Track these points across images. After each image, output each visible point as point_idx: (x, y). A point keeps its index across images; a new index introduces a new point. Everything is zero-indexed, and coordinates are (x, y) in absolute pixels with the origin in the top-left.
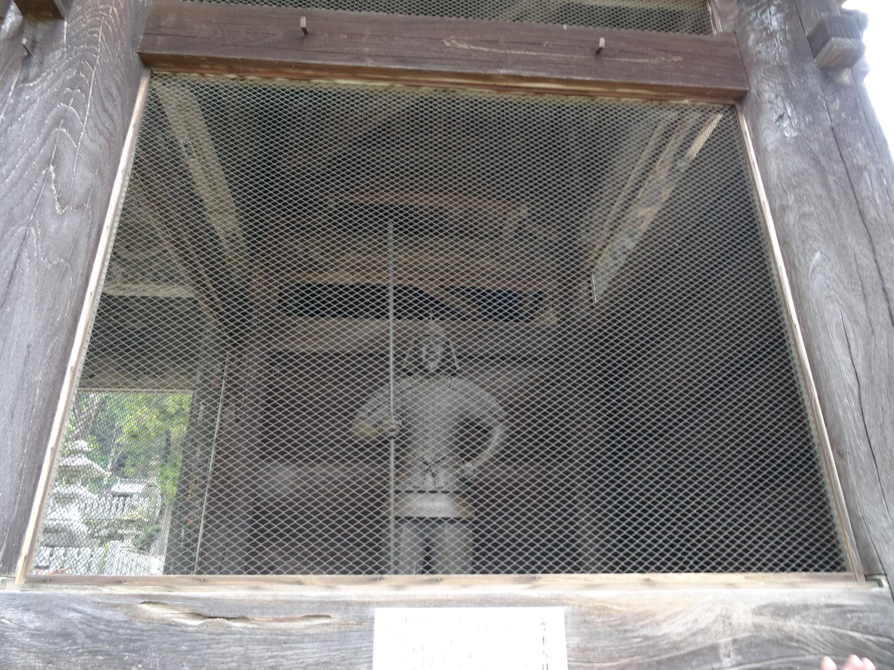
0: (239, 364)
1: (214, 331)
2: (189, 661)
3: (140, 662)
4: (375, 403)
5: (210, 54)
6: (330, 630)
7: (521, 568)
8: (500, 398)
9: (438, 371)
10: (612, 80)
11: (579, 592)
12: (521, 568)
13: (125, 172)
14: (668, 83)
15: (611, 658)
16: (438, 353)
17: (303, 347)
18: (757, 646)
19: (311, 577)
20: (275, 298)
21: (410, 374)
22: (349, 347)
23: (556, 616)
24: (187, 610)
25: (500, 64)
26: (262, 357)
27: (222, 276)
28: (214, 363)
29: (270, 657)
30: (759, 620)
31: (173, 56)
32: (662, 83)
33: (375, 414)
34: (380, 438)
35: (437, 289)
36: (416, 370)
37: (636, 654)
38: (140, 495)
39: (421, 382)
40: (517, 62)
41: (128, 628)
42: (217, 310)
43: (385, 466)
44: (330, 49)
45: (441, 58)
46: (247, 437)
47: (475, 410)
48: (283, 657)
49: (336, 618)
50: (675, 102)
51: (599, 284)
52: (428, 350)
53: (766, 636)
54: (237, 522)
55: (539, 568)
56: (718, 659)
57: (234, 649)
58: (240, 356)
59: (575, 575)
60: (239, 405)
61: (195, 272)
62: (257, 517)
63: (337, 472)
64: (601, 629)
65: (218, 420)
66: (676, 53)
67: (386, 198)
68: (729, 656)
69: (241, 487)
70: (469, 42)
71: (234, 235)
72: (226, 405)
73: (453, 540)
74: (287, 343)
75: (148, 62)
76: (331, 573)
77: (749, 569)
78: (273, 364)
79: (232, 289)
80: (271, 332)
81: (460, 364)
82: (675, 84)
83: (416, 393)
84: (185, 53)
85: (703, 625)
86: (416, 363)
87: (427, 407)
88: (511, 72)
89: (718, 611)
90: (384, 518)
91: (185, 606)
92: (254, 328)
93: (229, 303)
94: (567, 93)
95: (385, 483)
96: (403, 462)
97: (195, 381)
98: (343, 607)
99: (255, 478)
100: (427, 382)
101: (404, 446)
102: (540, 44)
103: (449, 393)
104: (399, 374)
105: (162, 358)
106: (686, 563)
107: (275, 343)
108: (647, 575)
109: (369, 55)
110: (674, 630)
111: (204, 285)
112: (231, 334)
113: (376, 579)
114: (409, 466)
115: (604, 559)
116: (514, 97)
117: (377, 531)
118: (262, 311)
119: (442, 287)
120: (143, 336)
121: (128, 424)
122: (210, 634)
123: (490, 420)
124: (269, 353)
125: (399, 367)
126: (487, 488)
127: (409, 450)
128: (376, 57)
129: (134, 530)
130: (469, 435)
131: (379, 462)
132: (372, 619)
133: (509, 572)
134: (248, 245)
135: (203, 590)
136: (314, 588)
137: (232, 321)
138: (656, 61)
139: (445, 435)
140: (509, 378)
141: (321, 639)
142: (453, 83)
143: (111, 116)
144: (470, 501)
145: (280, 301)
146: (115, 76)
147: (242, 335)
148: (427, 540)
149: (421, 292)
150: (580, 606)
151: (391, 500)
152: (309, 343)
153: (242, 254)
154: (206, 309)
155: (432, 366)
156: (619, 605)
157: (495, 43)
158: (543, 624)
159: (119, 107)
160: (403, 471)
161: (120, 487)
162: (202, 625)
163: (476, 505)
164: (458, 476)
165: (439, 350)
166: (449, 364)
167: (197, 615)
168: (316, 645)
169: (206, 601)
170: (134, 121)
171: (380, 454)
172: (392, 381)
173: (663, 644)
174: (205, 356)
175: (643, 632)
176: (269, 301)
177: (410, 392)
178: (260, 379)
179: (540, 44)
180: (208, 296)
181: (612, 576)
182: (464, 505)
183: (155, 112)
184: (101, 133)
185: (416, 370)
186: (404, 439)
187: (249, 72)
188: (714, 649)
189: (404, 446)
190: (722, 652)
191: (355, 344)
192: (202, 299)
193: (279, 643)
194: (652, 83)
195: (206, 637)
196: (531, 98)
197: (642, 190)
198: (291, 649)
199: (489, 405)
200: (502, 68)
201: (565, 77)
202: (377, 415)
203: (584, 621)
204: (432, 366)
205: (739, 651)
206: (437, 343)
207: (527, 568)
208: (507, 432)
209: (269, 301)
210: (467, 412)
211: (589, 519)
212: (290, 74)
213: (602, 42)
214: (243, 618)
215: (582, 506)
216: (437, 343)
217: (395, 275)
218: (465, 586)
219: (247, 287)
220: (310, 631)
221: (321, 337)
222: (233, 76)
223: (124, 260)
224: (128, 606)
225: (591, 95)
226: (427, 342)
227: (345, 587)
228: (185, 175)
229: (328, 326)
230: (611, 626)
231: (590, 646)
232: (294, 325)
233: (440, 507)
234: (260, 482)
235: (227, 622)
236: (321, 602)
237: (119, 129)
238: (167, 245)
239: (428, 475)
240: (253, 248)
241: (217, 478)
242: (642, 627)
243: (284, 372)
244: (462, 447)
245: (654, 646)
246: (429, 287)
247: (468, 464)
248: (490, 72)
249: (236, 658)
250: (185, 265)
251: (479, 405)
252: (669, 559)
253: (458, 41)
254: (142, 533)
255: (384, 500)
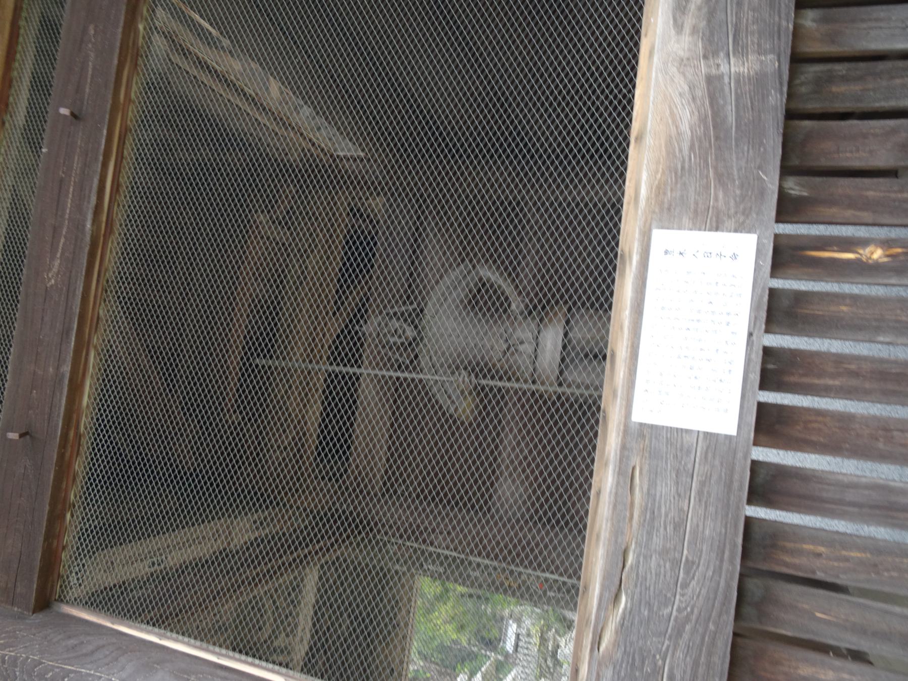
0: (391, 527)
1: (354, 550)
2: (659, 609)
3: (654, 656)
4: (442, 395)
5: (41, 539)
6: (646, 468)
7: (610, 268)
8: (451, 265)
9: (416, 327)
10: (109, 106)
11: (640, 212)
12: (610, 268)
13: (161, 636)
14: (118, 44)
15: (707, 187)
16: (397, 325)
17: (380, 459)
18: (712, 34)
19: (595, 481)
20: (326, 485)
21: (416, 357)
22: (386, 412)
23: (661, 238)
24: (611, 607)
25: (78, 226)
26: (386, 502)
27: (298, 537)
28: (388, 552)
29: (665, 529)
30: (687, 29)
31: (39, 577)
32: (117, 51)
33: (454, 397)
34: (478, 394)
35: (337, 320)
36: (413, 350)
37: (706, 162)
38: (519, 626)
39: (425, 345)
40: (79, 208)
41: (621, 666)
42: (332, 545)
43: (508, 391)
44: (47, 410)
45: (68, 291)
46: (467, 524)
47: (460, 293)
48: (666, 515)
49: (635, 460)
50: (141, 39)
51: (346, 148)
52: (393, 336)
53: (703, 24)
54: (551, 541)
55: (612, 249)
56: (720, 77)
57: (653, 564)
58: (383, 526)
59: (624, 213)
60: (434, 531)
61: (290, 565)
62: (549, 520)
63: (509, 439)
64: (678, 194)
65: (447, 552)
66: (85, 31)
67: (234, 361)
68: (718, 65)
69: (516, 535)
70: (53, 258)
71: (255, 522)
72: (432, 544)
73: (589, 330)
74: (374, 476)
75: (44, 602)
76: (593, 461)
77: (638, 32)
78: (395, 492)
79: (313, 528)
80: (361, 492)
81: (411, 303)
82: (119, 36)
83: (436, 353)
84: (37, 564)
85: (686, 88)
86: (406, 349)
87: (453, 342)
88: (90, 216)
89: (675, 70)
90: (559, 398)
91: (607, 609)
92: (355, 508)
93: (327, 532)
94: (120, 158)
95: (524, 393)
96: (506, 373)
97: (404, 574)
98: (626, 453)
99: (509, 520)
100: (426, 340)
101: (489, 371)
102: (61, 181)
103: (440, 318)
104: (415, 368)
105: (382, 600)
106: (624, 96)
107: (373, 488)
108: (632, 139)
109: (58, 368)
110: (686, 117)
111: (305, 556)
112: (360, 533)
113: (604, 417)
114: (510, 367)
115: (603, 181)
116: (120, 216)
117: (571, 406)
118: (338, 499)
119: (334, 314)
120: (356, 618)
121: (450, 633)
122: (636, 585)
123: (473, 279)
124: (383, 495)
125: (407, 367)
126: (541, 289)
127: (494, 365)
128: (60, 362)
129: (551, 634)
130: (484, 302)
131: (503, 397)
132: (641, 424)
133: (613, 281)
134: (267, 507)
135: (594, 589)
136: (606, 480)
137: (345, 530)
138: (92, 54)
139: (482, 327)
140: (434, 252)
141: (654, 477)
142: (98, 281)
143: (98, 648)
144: (552, 308)
145: (330, 479)
146: (55, 640)
147: (361, 522)
148: (586, 356)
149: (338, 337)
150: (654, 212)
151: (542, 389)
152: (377, 453)
153: (276, 515)
154: (330, 556)
155: (410, 333)
156: (657, 172)
157: (56, 230)
158: (666, 252)
159: (89, 638)
160: (514, 374)
161: (509, 646)
162: (626, 594)
163: (557, 303)
164: (525, 318)
165: (395, 324)
166: (410, 315)
167: (617, 598)
168: (658, 482)
169: (603, 588)
170: (109, 624)
171: (495, 396)
172: (421, 376)
173: (700, 132)
174: (379, 561)
175: (686, 151)
176: (329, 491)
177: (434, 358)
178: (409, 507)
179: (61, 181)
180: (317, 553)
181: (629, 175)
182: (555, 314)
183: (103, 601)
184: (116, 659)
185: (413, 350)
186: (479, 369)
187: (66, 498)
188: (710, 80)
189: (489, 371)
190: (714, 71)
191: (383, 406)
192: (319, 559)
193: (653, 519)
194: (116, 62)
195: (638, 589)
196: (123, 198)
197: (246, 89)
198: (660, 507)
199: (457, 278)
200: (84, 226)
201: (101, 158)
202: (455, 395)
203: (668, 213)
204: (410, 333)
205: (715, 54)
206: (386, 325)
207: (611, 262)
208: (487, 261)
209: (329, 491)
210: (462, 301)
211: (593, 187)
212: (71, 457)
213: (64, 111)
214: (625, 553)
215: (597, 193)
216: (386, 325)
217: (318, 363)
218: (622, 328)
219: (312, 512)
220: (645, 487)
221: (300, 468)
222: (68, 516)
223: (273, 631)
224: (600, 664)
225: (125, 131)
226: (385, 335)
227: (607, 448)
228: (182, 570)
229: (362, 432)
230: (676, 183)
231: (692, 207)
232: (357, 467)
233: (551, 339)
234: (514, 514)
235: (626, 569)
236: (619, 474)
237: (114, 640)
238: (260, 590)
239: (521, 348)
240: (271, 502)
241: (505, 558)
242: (681, 151)
243: (404, 481)
244: (497, 310)
245: (700, 141)
246: (335, 326)
247: (513, 306)
248: (88, 239)
249: (662, 563)
250: (282, 575)
251: (455, 288)
252: (619, 114)
253: (50, 270)
254: (557, 625)
255: (541, 396)
